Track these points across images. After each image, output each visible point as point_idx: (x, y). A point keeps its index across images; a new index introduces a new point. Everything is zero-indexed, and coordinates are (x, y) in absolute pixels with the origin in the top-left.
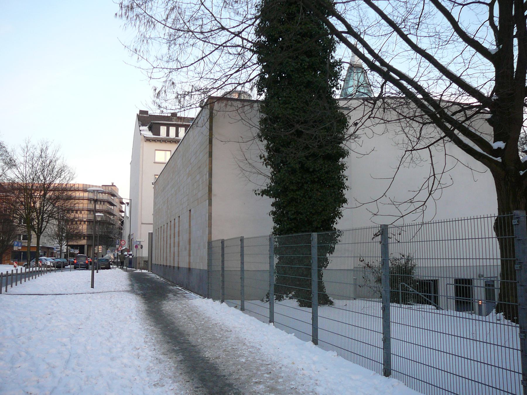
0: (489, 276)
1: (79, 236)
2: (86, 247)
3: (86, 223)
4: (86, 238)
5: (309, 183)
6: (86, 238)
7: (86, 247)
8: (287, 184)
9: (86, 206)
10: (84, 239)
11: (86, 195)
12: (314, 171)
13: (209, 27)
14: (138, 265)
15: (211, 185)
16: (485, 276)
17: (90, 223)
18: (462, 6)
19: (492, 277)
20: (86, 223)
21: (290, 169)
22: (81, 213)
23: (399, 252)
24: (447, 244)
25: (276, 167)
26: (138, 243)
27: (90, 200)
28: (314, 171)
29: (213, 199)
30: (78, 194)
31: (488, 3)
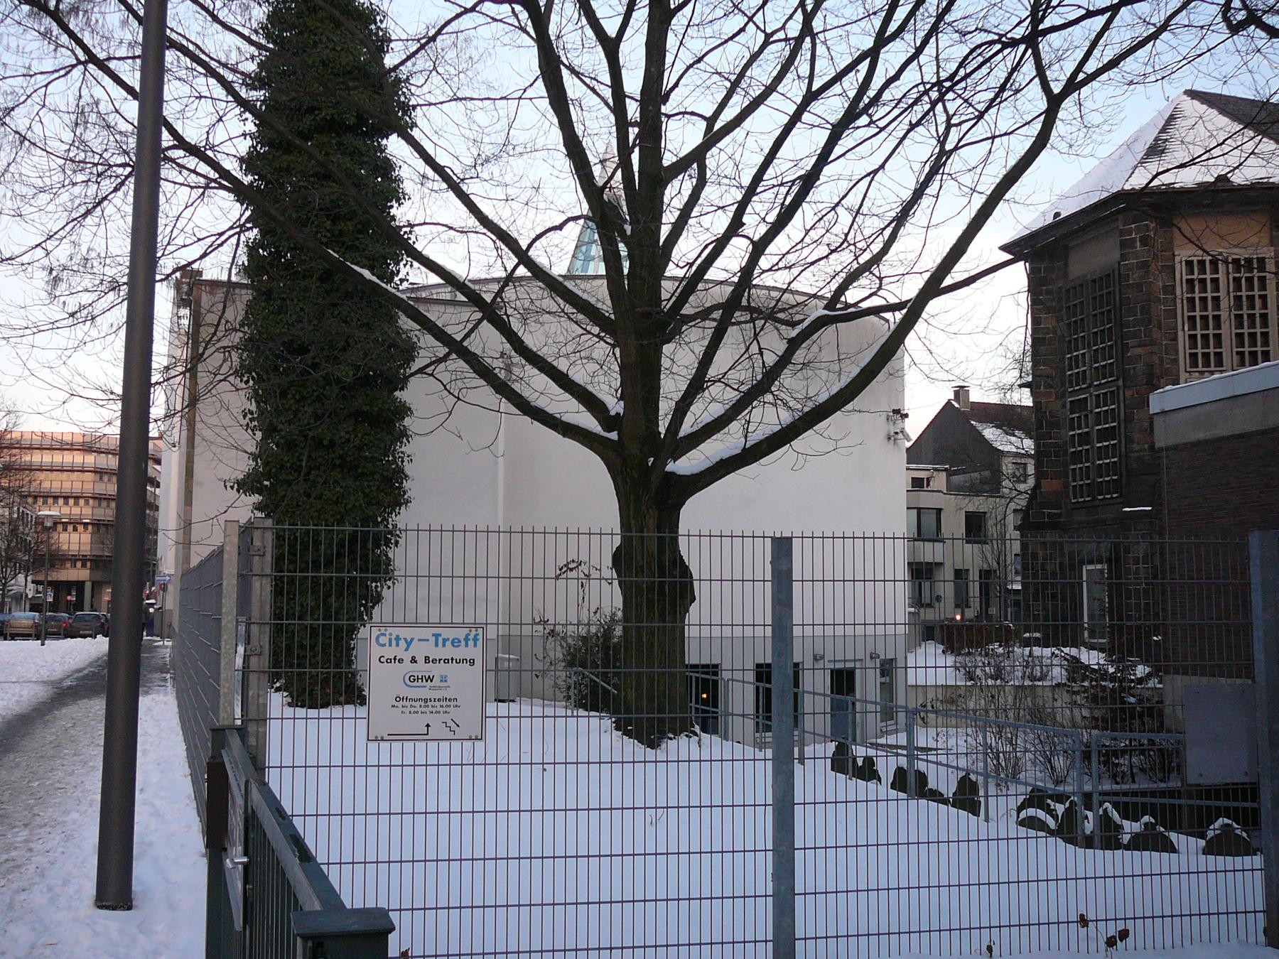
0: (840, 656)
1: (59, 559)
2: (88, 587)
3: (90, 527)
4: (88, 564)
5: (323, 468)
6: (88, 564)
7: (88, 587)
8: (274, 470)
9: (89, 488)
10: (84, 566)
11: (90, 459)
12: (332, 444)
13: (202, 80)
14: (166, 629)
15: (193, 462)
16: (829, 656)
17: (99, 530)
18: (1057, 88)
19: (848, 661)
20: (90, 527)
21: (282, 441)
22: (76, 504)
23: (942, 604)
24: (839, 594)
25: (269, 431)
26: (168, 578)
27: (101, 473)
28: (332, 444)
29: (195, 490)
30: (36, 458)
31: (708, 116)
